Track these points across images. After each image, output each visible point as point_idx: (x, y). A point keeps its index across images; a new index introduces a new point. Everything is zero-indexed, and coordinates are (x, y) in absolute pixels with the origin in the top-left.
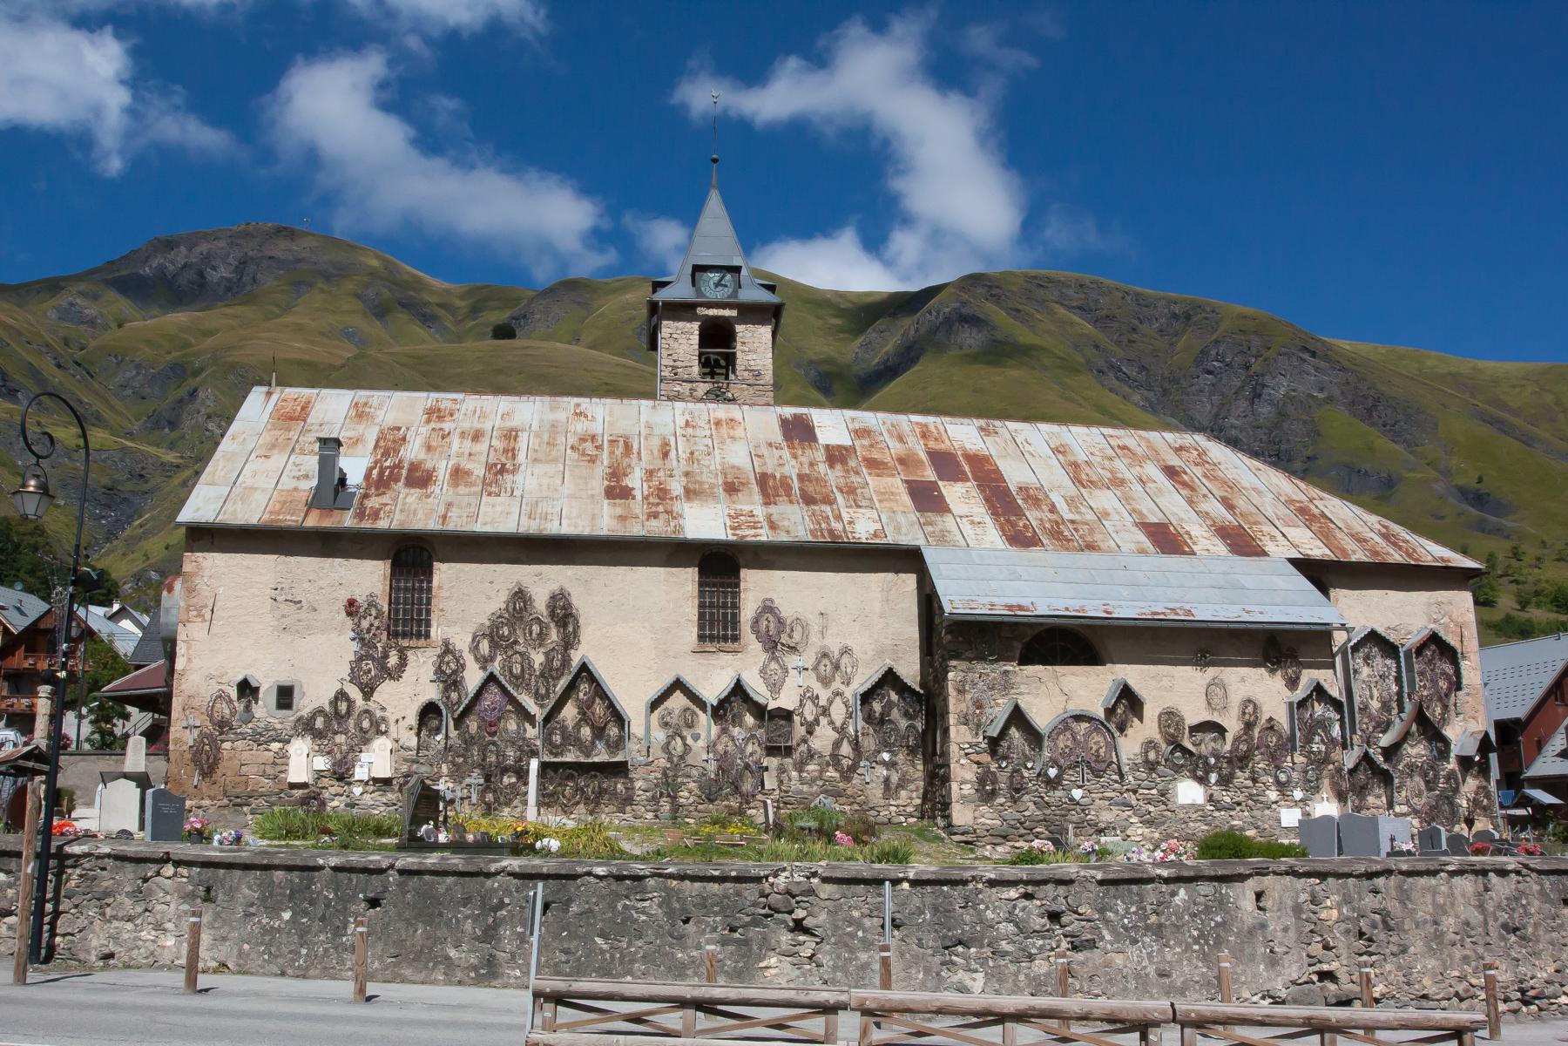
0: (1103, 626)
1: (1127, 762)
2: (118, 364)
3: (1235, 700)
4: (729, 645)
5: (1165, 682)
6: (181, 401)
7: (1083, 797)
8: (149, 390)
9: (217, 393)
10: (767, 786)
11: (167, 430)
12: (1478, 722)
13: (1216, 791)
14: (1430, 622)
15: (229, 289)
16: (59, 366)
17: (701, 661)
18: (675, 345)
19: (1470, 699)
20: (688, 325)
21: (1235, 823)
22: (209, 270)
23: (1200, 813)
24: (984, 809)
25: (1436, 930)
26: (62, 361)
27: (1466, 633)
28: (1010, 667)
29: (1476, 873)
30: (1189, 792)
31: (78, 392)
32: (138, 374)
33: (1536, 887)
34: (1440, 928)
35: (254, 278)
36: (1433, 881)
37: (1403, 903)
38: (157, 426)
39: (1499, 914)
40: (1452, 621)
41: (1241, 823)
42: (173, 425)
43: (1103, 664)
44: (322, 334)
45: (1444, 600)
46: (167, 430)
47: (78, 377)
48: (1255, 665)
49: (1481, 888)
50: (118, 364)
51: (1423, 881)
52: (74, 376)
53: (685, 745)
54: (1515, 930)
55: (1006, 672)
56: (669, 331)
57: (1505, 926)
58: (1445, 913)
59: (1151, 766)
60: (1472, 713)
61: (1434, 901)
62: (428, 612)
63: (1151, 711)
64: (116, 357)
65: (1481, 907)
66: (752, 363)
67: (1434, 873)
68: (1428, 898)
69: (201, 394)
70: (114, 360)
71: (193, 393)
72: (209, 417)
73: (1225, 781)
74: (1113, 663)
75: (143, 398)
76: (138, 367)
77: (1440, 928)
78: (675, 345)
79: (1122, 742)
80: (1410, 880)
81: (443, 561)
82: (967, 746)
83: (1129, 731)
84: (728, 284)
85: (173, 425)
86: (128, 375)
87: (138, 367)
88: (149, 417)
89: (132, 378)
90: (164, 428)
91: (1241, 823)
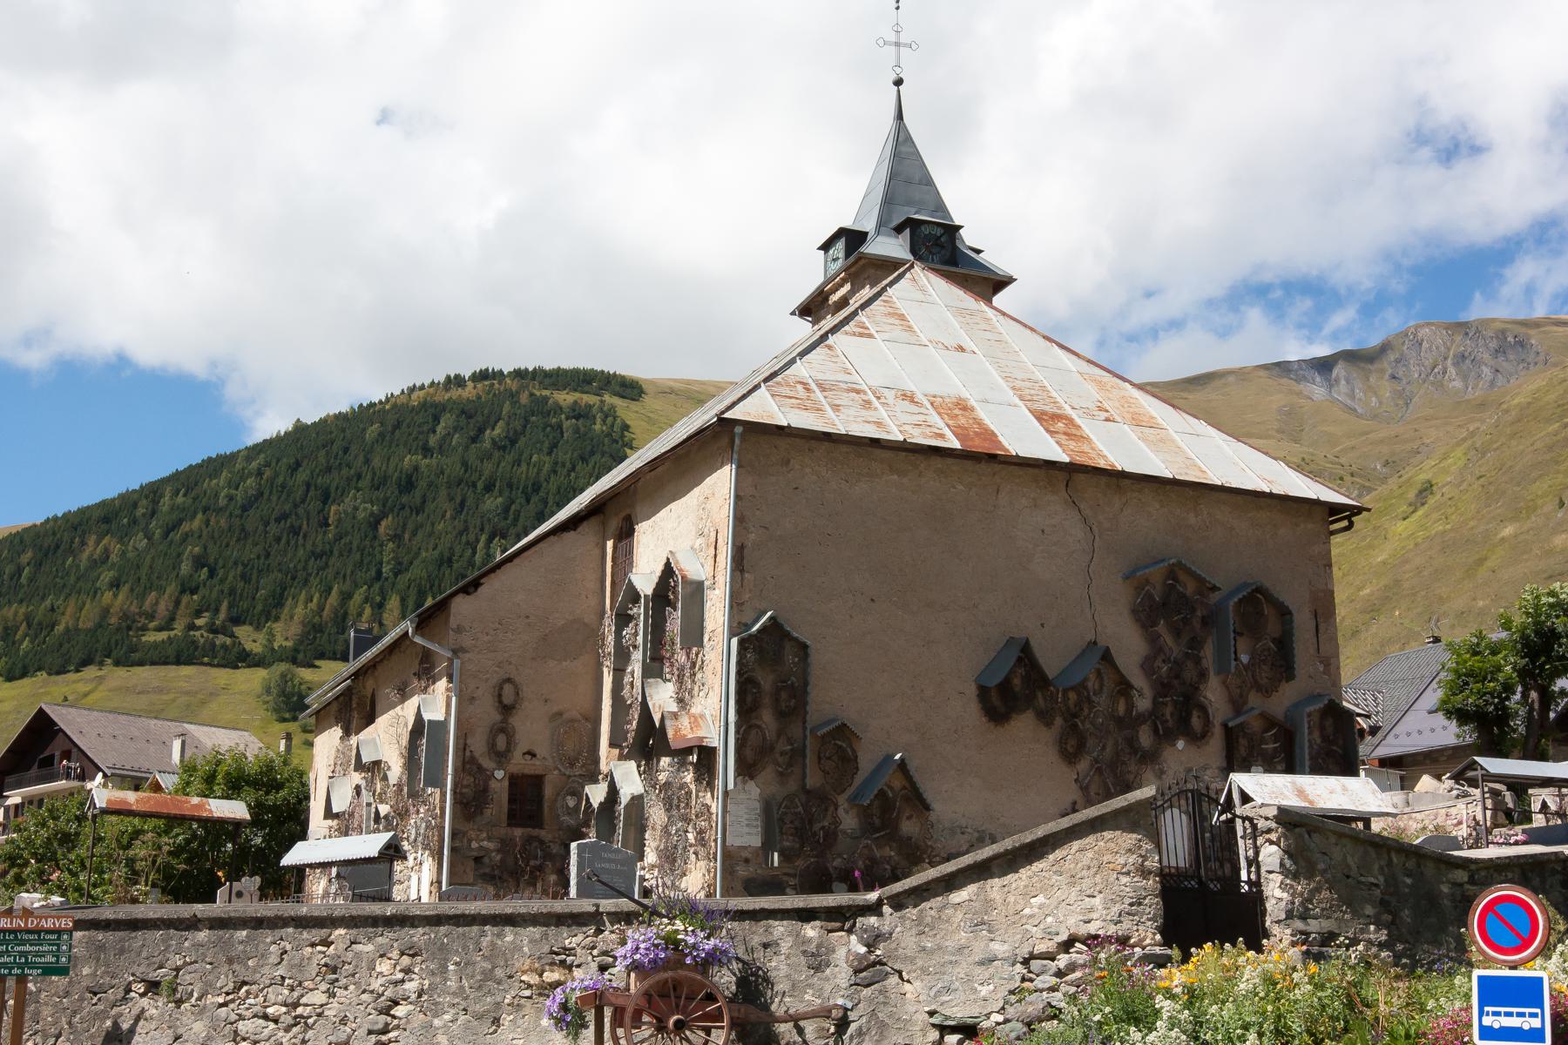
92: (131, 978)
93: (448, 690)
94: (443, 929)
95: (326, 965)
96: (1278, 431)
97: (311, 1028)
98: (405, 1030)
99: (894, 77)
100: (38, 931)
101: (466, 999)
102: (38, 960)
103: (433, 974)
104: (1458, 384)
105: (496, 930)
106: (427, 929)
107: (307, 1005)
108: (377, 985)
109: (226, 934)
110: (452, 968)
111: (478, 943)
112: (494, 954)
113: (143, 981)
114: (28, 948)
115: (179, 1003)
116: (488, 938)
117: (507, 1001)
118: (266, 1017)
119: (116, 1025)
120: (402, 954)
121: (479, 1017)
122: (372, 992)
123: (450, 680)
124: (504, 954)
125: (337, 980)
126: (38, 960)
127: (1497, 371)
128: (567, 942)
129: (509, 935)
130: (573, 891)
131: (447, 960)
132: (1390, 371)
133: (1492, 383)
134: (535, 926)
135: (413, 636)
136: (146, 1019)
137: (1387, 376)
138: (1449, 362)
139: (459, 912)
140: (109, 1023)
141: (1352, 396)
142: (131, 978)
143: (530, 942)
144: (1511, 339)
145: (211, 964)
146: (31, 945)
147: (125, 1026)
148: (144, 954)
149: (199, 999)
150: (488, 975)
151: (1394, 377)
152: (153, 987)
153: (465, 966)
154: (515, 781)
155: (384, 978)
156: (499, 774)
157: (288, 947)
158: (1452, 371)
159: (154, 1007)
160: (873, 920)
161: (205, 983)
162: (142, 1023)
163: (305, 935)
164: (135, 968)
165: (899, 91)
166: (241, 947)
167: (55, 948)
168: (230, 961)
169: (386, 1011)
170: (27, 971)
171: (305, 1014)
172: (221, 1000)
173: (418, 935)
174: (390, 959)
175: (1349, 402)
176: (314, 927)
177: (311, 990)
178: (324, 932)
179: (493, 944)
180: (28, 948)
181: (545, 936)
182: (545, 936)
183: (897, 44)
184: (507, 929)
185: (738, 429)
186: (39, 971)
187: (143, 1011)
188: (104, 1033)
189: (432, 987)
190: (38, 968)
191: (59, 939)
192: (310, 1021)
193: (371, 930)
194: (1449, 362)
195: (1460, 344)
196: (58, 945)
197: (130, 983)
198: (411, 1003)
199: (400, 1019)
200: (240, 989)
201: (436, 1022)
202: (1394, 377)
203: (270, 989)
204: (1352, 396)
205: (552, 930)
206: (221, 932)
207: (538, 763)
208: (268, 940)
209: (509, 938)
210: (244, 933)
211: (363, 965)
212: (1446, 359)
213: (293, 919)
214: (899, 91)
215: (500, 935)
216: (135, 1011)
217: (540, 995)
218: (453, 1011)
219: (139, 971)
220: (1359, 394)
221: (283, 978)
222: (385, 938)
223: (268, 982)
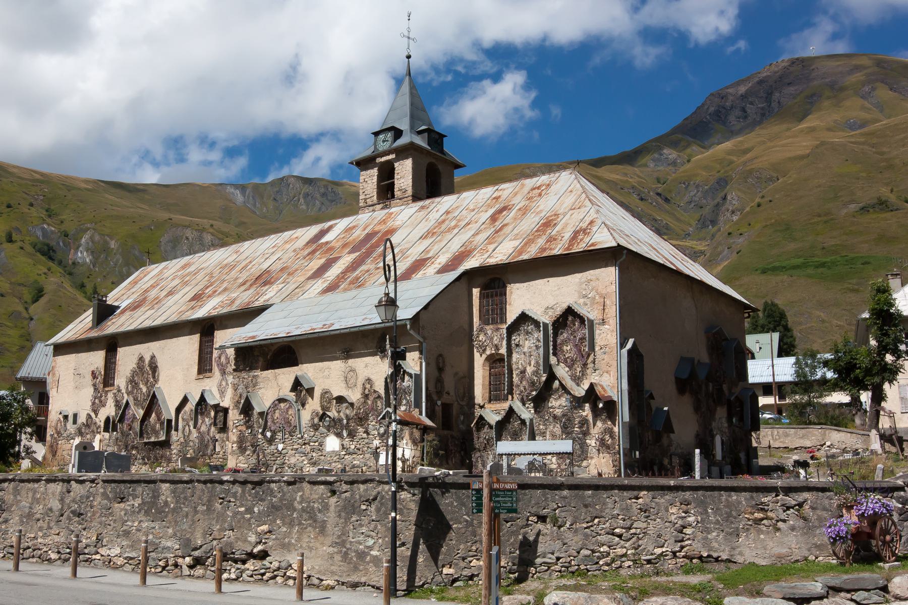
0: (300, 340)
1: (305, 425)
2: (686, 188)
3: (361, 380)
4: (208, 374)
5: (326, 373)
6: (718, 205)
7: (283, 449)
8: (705, 201)
9: (739, 194)
10: (217, 450)
11: (710, 227)
12: (610, 376)
13: (347, 442)
14: (580, 298)
15: (763, 115)
16: (642, 199)
17: (199, 384)
18: (366, 186)
19: (606, 357)
20: (372, 171)
21: (355, 462)
22: (748, 105)
23: (338, 457)
24: (241, 458)
25: (30, 512)
26: (643, 195)
27: (608, 302)
28: (258, 373)
29: (63, 481)
30: (332, 443)
31: (654, 214)
32: (698, 191)
33: (102, 490)
34: (32, 511)
35: (779, 102)
36: (36, 485)
37: (15, 496)
38: (704, 226)
39: (72, 504)
40: (598, 294)
41: (358, 462)
42: (714, 222)
43: (297, 365)
44: (829, 129)
45: (593, 278)
46: (710, 227)
47: (654, 203)
48: (373, 354)
49: (65, 490)
50: (686, 188)
51: (30, 485)
52: (652, 204)
53: (190, 430)
54: (80, 515)
55: (254, 377)
56: (363, 177)
57: (73, 512)
58: (38, 503)
59: (316, 427)
60: (606, 368)
61: (33, 496)
62: (114, 374)
63: (317, 393)
64: (684, 183)
65: (62, 500)
66: (402, 185)
67: (37, 481)
68: (30, 494)
69: (729, 197)
70: (684, 186)
71: (725, 198)
72: (733, 212)
73: (352, 435)
74: (302, 364)
75: (701, 207)
76: (697, 186)
77: (32, 511)
78: (366, 186)
79: (303, 412)
80: (23, 484)
81: (120, 347)
82: (237, 422)
83: (307, 406)
84: (389, 139)
85: (714, 222)
86: (692, 194)
87: (697, 186)
88: (699, 221)
89: (695, 196)
90: (708, 226)
91: (358, 462)
92: (529, 514)
93: (420, 358)
94: (700, 493)
95: (640, 509)
96: (219, 218)
97: (641, 540)
98: (694, 540)
99: (406, 54)
100: (505, 490)
101: (722, 525)
102: (504, 505)
103: (702, 514)
104: (304, 207)
105: (727, 493)
106: (691, 492)
107: (636, 528)
108: (673, 519)
109: (581, 492)
110: (710, 511)
111: (720, 499)
112: (729, 505)
113: (535, 515)
114: (500, 499)
115: (560, 527)
116: (724, 497)
117: (741, 527)
118: (613, 534)
119: (524, 537)
120: (681, 504)
121: (731, 534)
122: (670, 522)
123: (421, 353)
124: (734, 505)
125: (649, 516)
126: (504, 505)
127: (323, 203)
128: (763, 500)
129: (734, 497)
130: (697, 475)
131: (707, 507)
132: (273, 196)
133: (320, 209)
134: (746, 492)
135: (410, 330)
136: (543, 535)
137: (272, 198)
138: (301, 196)
139: (710, 485)
140: (520, 537)
141: (255, 205)
142: (529, 514)
143: (745, 499)
144: (330, 190)
145: (574, 507)
146: (502, 497)
147: (531, 539)
148: (533, 502)
149: (572, 525)
150: (729, 515)
151: (275, 199)
152: (542, 519)
153: (717, 511)
154: (443, 404)
155: (675, 516)
156: (439, 403)
157: (617, 500)
158: (302, 200)
159: (547, 528)
160: (902, 493)
161: (574, 517)
162: (541, 537)
163: (625, 494)
164: (530, 509)
165: (409, 61)
166: (590, 499)
167: (511, 499)
168: (586, 506)
169: (681, 532)
170: (501, 511)
171: (637, 533)
172: (585, 525)
173: (688, 495)
174: (676, 506)
175: (253, 208)
176: (629, 490)
177: (635, 521)
178: (635, 493)
179: (727, 500)
180: (500, 499)
181: (752, 497)
182: (752, 497)
183: (409, 38)
184: (733, 493)
185: (625, 252)
186: (506, 511)
187: (540, 531)
188: (519, 543)
189: (703, 521)
190: (505, 509)
191: (512, 494)
192: (640, 536)
193: (661, 492)
194: (301, 196)
195: (306, 189)
196: (512, 497)
197: (528, 517)
198: (693, 527)
199: (689, 535)
200: (594, 520)
201: (709, 536)
202: (275, 199)
203: (612, 520)
204: (255, 205)
205: (755, 495)
206: (576, 492)
207: (450, 398)
208: (605, 496)
209: (734, 498)
210: (590, 492)
211: (662, 509)
212: (300, 194)
213: (616, 486)
214: (409, 61)
215: (730, 496)
216: (535, 531)
217: (755, 524)
218: (717, 531)
219: (533, 510)
220: (258, 205)
221: (618, 515)
222: (669, 496)
223: (610, 517)
